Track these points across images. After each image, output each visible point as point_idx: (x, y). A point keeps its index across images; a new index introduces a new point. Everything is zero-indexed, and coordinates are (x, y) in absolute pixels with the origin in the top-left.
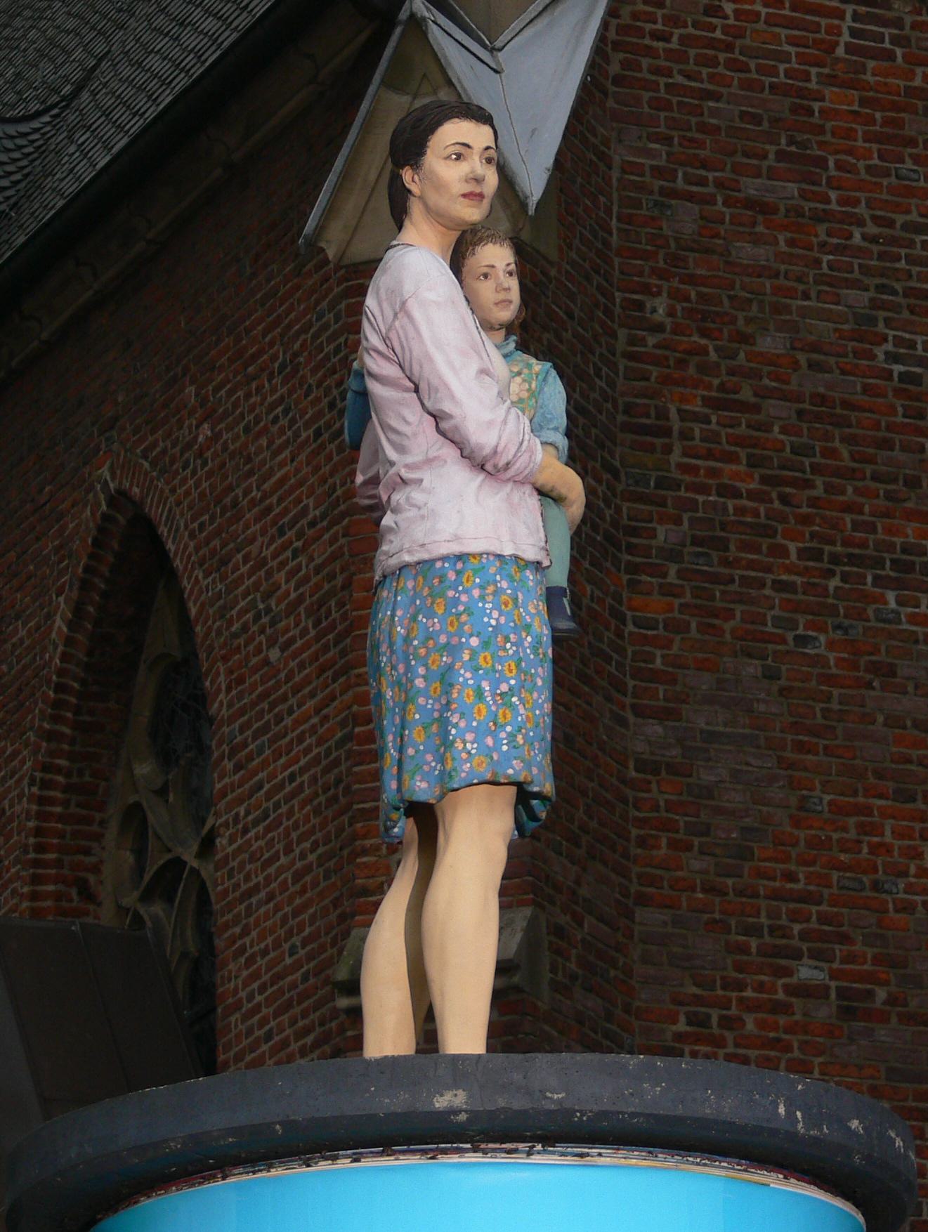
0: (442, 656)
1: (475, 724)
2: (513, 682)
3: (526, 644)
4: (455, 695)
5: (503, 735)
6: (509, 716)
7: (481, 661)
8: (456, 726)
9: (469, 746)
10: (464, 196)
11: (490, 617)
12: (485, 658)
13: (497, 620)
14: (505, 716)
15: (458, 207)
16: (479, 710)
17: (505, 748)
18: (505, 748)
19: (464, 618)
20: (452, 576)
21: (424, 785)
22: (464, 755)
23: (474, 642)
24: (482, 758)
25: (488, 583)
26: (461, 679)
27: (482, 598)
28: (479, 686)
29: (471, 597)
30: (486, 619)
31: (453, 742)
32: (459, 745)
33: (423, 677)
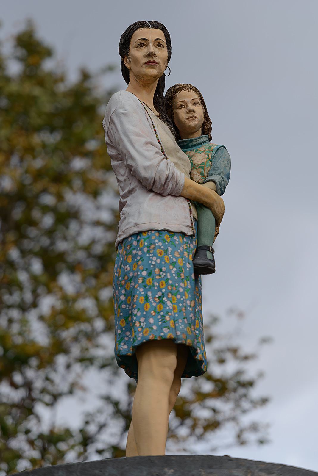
0: (131, 283)
1: (145, 313)
2: (164, 290)
3: (173, 272)
4: (135, 301)
5: (159, 317)
6: (162, 307)
7: (147, 282)
8: (136, 315)
9: (142, 324)
10: (146, 63)
11: (152, 260)
12: (149, 280)
13: (155, 261)
14: (160, 308)
15: (144, 69)
16: (147, 306)
17: (160, 323)
18: (160, 323)
19: (140, 263)
20: (135, 243)
21: (125, 347)
22: (140, 329)
23: (144, 273)
24: (148, 329)
25: (151, 244)
26: (138, 292)
27: (149, 252)
28: (147, 295)
29: (143, 252)
30: (150, 262)
31: (135, 323)
32: (137, 324)
33: (124, 294)
